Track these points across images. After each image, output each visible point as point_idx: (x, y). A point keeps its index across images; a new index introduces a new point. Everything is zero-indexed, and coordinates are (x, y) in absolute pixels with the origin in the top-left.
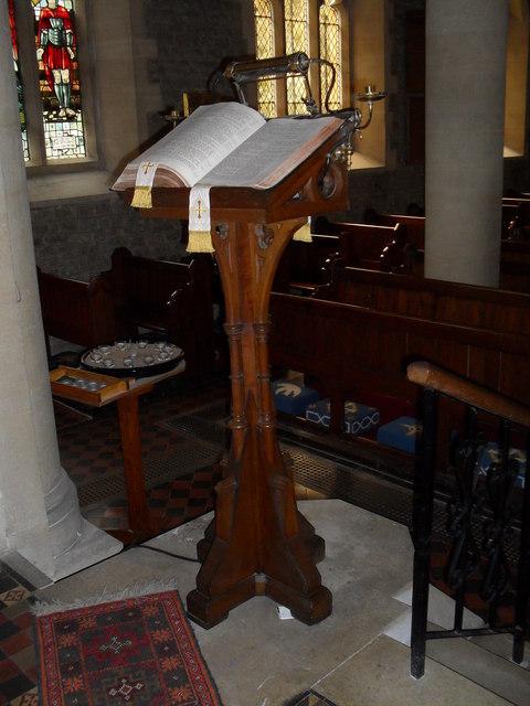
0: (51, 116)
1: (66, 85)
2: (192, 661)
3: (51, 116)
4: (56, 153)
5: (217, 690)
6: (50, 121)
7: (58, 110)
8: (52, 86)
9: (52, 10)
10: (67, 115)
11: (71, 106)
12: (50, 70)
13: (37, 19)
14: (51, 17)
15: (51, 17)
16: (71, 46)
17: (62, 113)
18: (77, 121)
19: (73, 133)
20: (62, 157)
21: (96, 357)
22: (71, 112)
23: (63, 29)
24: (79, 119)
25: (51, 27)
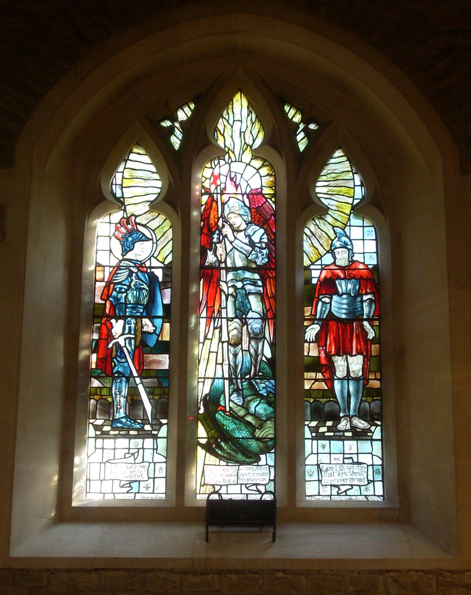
0: (323, 429)
1: (357, 379)
2: (105, 397)
3: (323, 429)
4: (327, 491)
5: (161, 570)
6: (320, 437)
7: (337, 420)
8: (330, 381)
9: (342, 268)
10: (353, 429)
11: (362, 415)
12: (329, 357)
13: (314, 281)
14: (339, 278)
15: (339, 278)
16: (370, 320)
17: (343, 425)
18: (372, 440)
19: (362, 458)
20: (338, 498)
21: (103, 258)
22: (361, 424)
23: (359, 294)
24: (377, 434)
25: (337, 293)
